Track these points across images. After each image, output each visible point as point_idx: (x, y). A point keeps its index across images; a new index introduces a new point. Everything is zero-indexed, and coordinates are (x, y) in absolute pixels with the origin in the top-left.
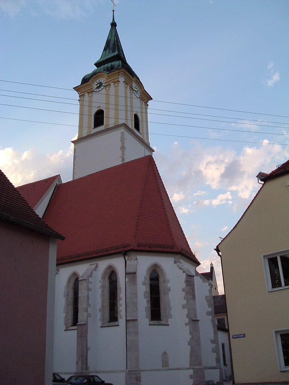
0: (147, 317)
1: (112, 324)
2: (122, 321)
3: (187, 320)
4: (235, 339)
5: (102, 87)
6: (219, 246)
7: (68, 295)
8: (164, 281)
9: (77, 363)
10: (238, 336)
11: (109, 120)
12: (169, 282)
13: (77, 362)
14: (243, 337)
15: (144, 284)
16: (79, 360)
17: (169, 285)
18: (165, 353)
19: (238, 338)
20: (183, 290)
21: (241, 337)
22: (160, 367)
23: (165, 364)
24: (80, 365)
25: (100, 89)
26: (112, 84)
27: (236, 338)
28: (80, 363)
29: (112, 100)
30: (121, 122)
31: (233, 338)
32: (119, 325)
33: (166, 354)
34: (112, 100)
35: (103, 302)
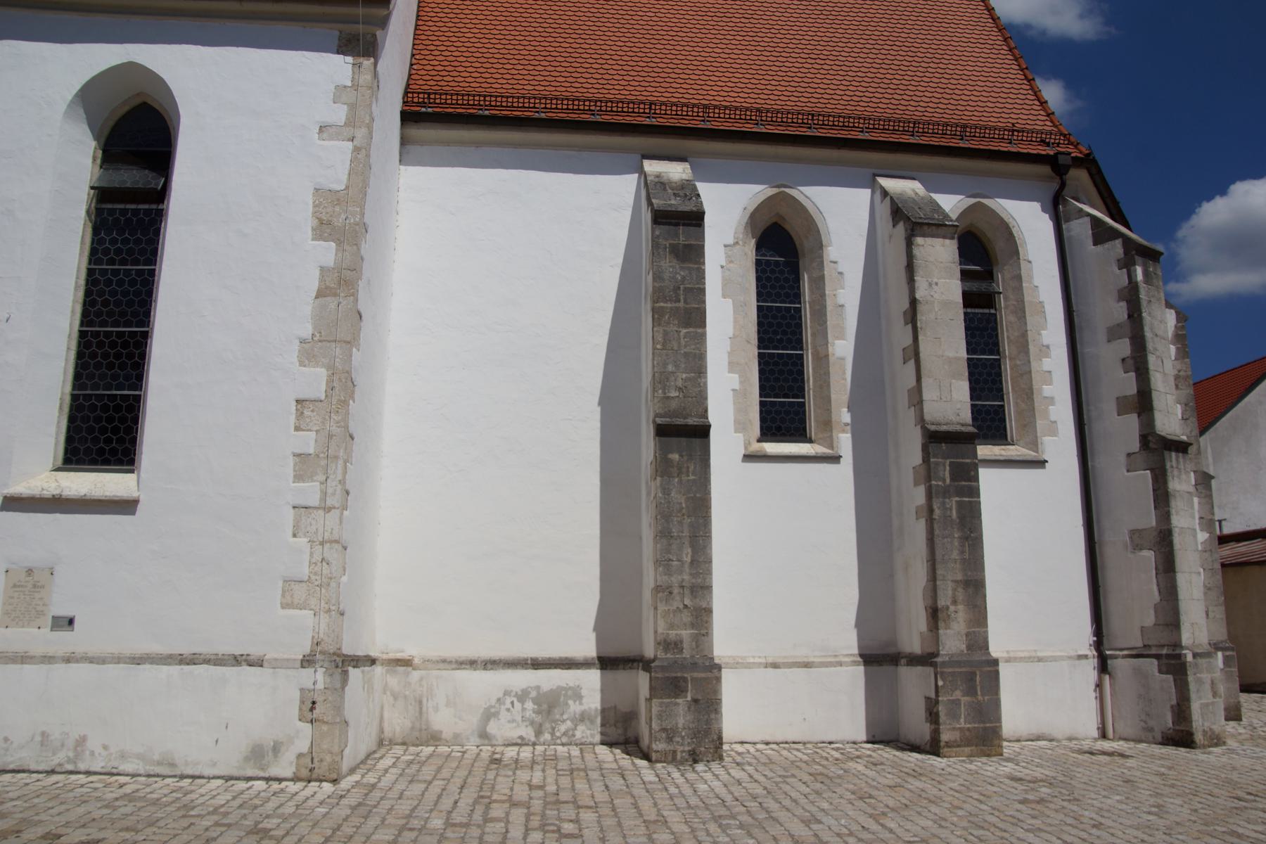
16: (955, 602)
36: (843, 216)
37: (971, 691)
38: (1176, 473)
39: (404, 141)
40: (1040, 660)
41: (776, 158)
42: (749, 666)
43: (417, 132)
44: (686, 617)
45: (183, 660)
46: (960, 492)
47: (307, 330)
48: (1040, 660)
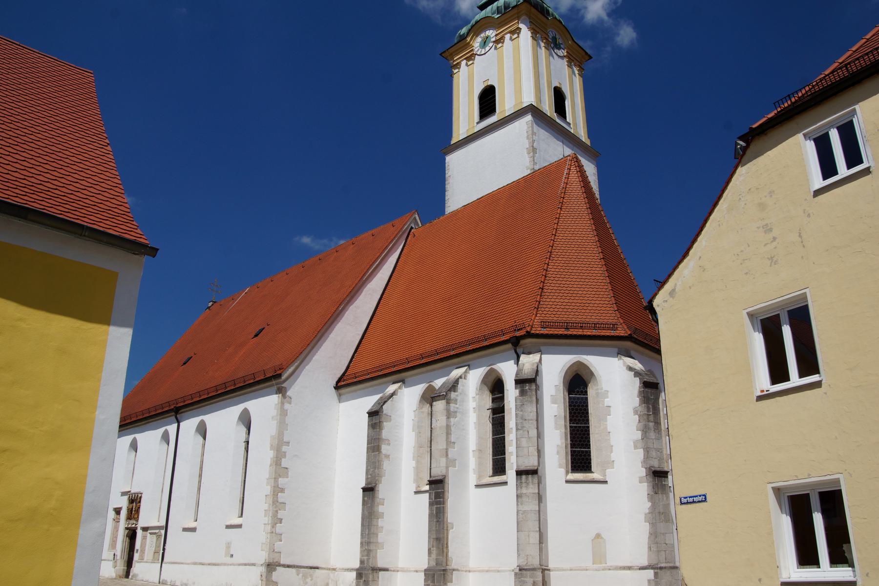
0: (560, 466)
1: (497, 479)
2: (511, 475)
3: (643, 472)
4: (684, 506)
5: (491, 45)
6: (245, 430)
7: (419, 427)
8: (598, 394)
9: (430, 552)
10: (691, 500)
11: (505, 105)
12: (607, 397)
13: (429, 550)
14: (702, 501)
15: (554, 401)
17: (607, 402)
18: (598, 536)
19: (690, 503)
20: (636, 412)
21: (699, 502)
22: (589, 564)
23: (599, 556)
24: (434, 556)
25: (487, 49)
26: (508, 36)
27: (688, 503)
28: (434, 552)
29: (508, 63)
30: (529, 99)
31: (682, 503)
32: (605, 482)
33: (602, 538)
34: (508, 63)
35: (480, 438)
36: (508, 370)
37: (433, 581)
38: (524, 485)
39: (339, 396)
40: (498, 571)
41: (428, 371)
42: (410, 571)
43: (343, 391)
44: (366, 553)
45: (245, 565)
46: (437, 503)
47: (267, 476)
48: (498, 571)
